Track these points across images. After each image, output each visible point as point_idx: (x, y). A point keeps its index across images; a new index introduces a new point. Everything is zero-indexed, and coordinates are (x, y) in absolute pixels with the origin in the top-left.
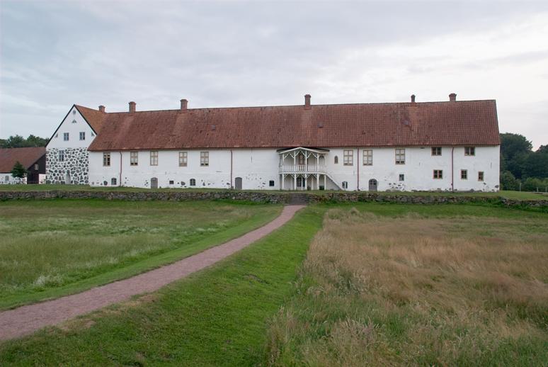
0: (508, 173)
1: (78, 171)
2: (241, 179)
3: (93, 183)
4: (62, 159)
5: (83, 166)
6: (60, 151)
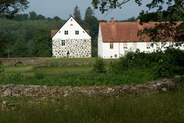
1: (75, 51)
2: (104, 42)
3: (105, 57)
4: (63, 44)
5: (78, 48)
6: (62, 41)
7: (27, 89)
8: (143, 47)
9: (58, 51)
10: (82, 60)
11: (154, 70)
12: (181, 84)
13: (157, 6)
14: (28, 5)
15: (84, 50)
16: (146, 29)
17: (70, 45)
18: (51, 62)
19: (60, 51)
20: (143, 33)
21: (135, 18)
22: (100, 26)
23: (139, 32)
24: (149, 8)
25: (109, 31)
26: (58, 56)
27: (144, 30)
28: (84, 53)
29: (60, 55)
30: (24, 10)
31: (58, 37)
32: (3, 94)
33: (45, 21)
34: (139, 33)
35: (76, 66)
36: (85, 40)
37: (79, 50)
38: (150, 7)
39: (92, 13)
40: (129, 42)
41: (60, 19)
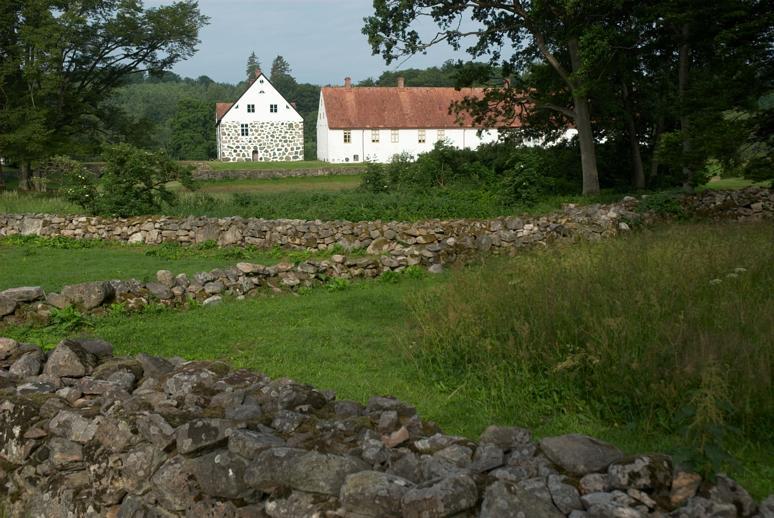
0: (213, 137)
1: (269, 147)
2: (331, 128)
4: (245, 132)
6: (242, 126)
7: (280, 228)
8: (466, 139)
9: (231, 147)
10: (286, 166)
11: (504, 186)
12: (651, 214)
13: (489, 52)
14: (195, 47)
15: (289, 145)
16: (466, 100)
17: (259, 135)
18: (223, 171)
19: (238, 147)
20: (461, 108)
21: (374, 81)
22: (322, 98)
23: (452, 105)
24: (472, 56)
25: (342, 106)
26: (234, 159)
27: (462, 103)
28: (289, 151)
29: (238, 155)
30: (187, 56)
31: (234, 117)
32: (223, 238)
33: (182, 84)
34: (454, 108)
35: (275, 179)
36: (291, 125)
37: (277, 145)
38: (474, 54)
39: (285, 69)
40: (382, 129)
41: (212, 82)
